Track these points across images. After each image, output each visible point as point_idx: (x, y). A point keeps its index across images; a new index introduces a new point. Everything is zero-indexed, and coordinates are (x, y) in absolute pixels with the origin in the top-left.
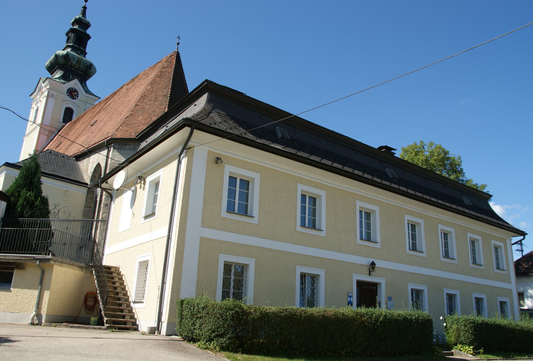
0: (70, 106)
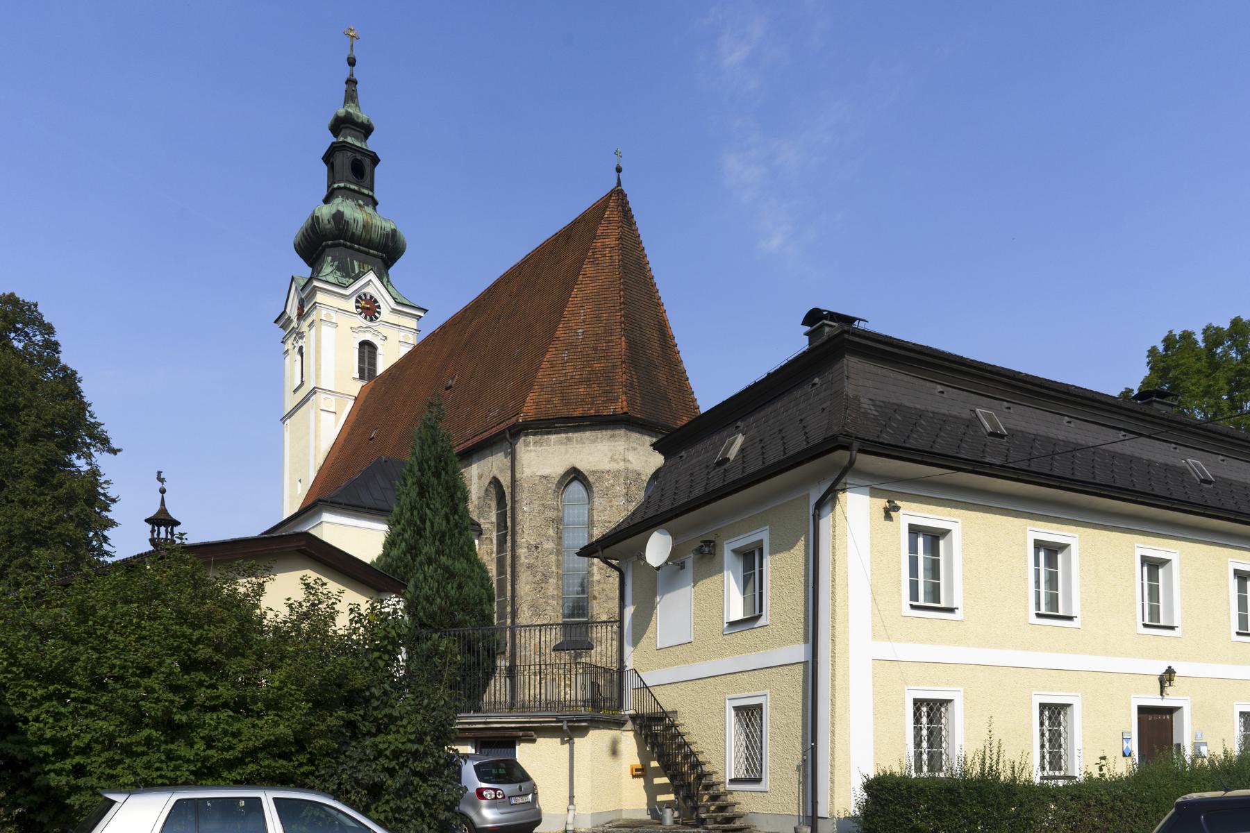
0: (368, 337)
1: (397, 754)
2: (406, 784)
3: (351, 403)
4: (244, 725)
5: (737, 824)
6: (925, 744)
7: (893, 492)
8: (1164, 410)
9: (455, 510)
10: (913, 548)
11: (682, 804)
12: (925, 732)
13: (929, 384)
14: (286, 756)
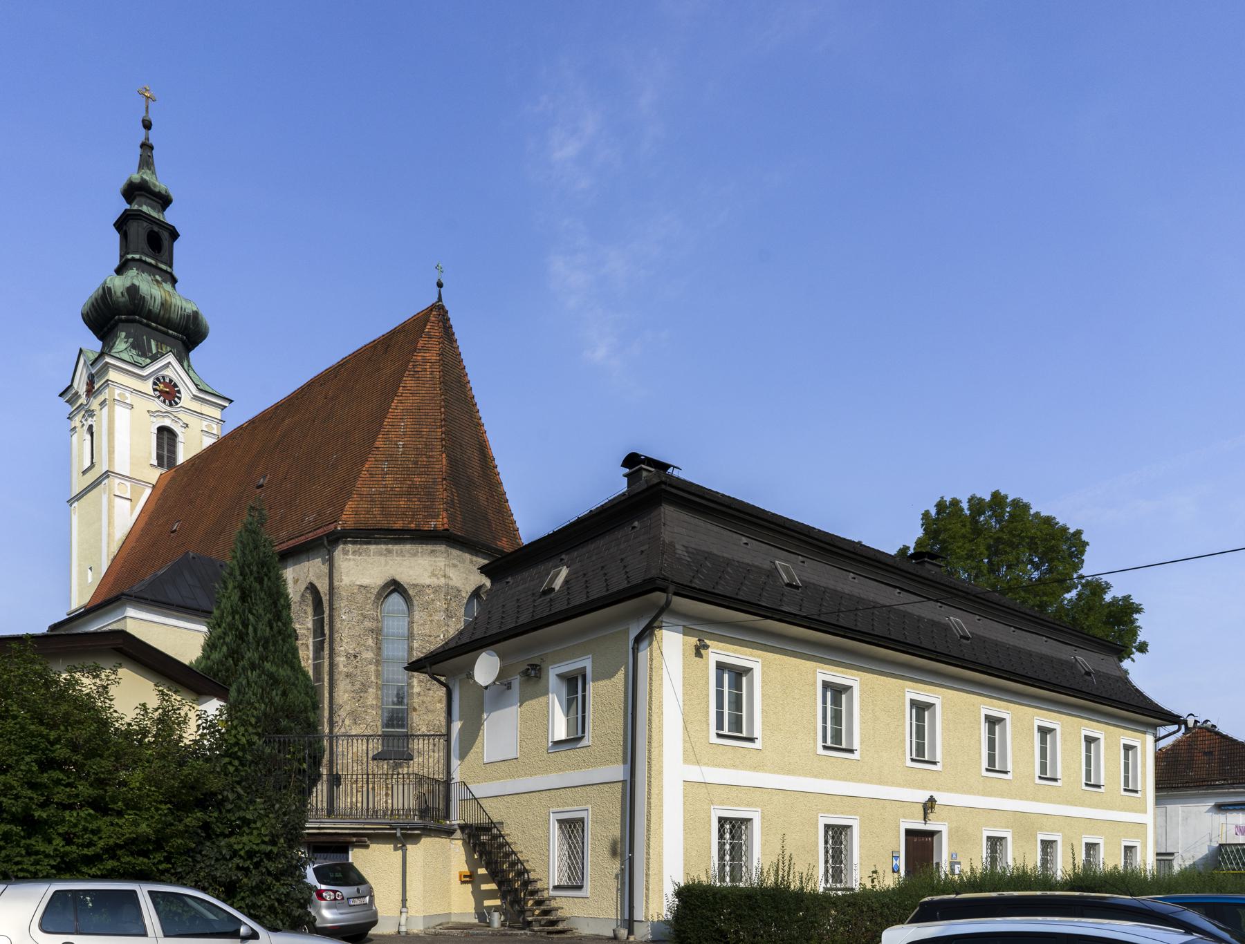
0: (167, 422)
1: (251, 854)
2: (262, 882)
3: (148, 491)
4: (102, 823)
5: (561, 926)
6: (727, 858)
7: (701, 631)
8: (934, 570)
9: (278, 616)
10: (720, 683)
11: (509, 908)
12: (727, 847)
13: (735, 536)
14: (145, 854)
